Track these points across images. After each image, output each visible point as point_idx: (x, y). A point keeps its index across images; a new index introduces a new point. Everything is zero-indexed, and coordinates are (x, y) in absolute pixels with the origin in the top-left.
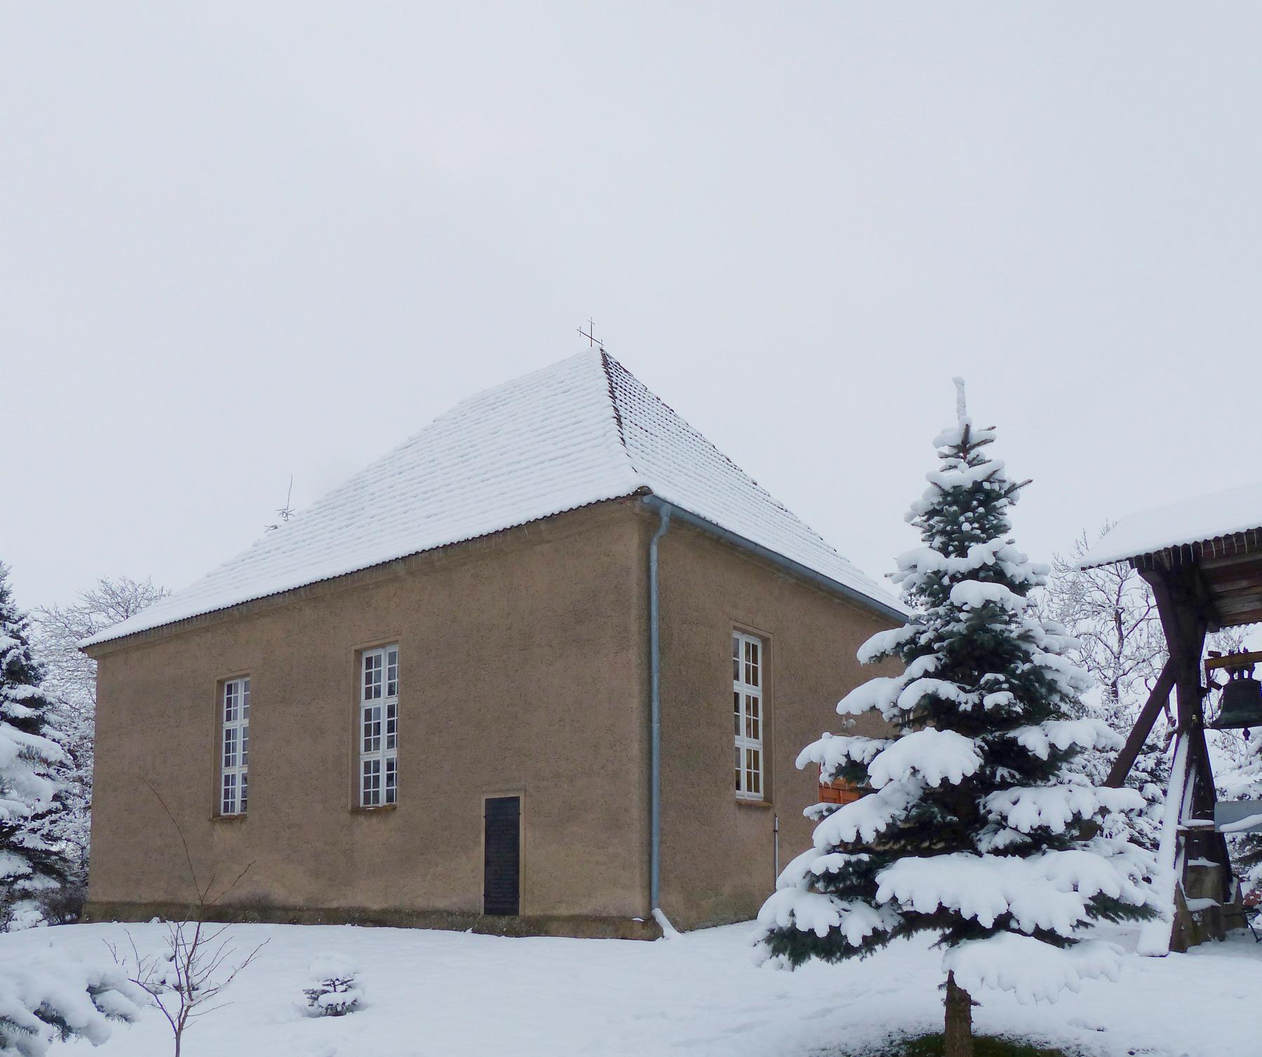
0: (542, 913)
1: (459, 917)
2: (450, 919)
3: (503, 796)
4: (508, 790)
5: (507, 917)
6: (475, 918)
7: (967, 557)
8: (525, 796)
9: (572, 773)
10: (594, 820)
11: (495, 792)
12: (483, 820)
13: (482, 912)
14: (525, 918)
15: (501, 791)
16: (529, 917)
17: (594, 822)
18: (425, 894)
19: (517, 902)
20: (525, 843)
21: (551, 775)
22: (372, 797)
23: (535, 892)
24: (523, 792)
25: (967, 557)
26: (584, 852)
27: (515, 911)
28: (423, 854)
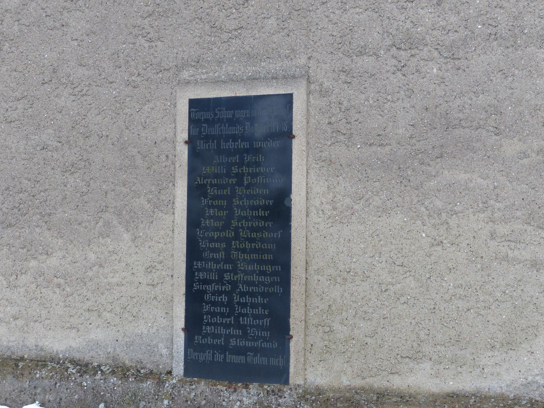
0: (358, 383)
1: (114, 380)
2: (87, 381)
3: (241, 92)
4: (253, 79)
5: (254, 388)
6: (160, 383)
7: (189, 99)
8: (309, 93)
9: (453, 36)
10: (526, 156)
11: (217, 82)
12: (183, 152)
13: (179, 369)
14: (305, 392)
15: (232, 80)
16: (319, 391)
17: (526, 161)
18: (16, 318)
19: (285, 352)
20: (308, 208)
21: (388, 42)
22: (274, 274)
23: (337, 326)
24: (305, 82)
25: (189, 99)
26: (493, 236)
27: (286, 382)
28: (10, 225)
